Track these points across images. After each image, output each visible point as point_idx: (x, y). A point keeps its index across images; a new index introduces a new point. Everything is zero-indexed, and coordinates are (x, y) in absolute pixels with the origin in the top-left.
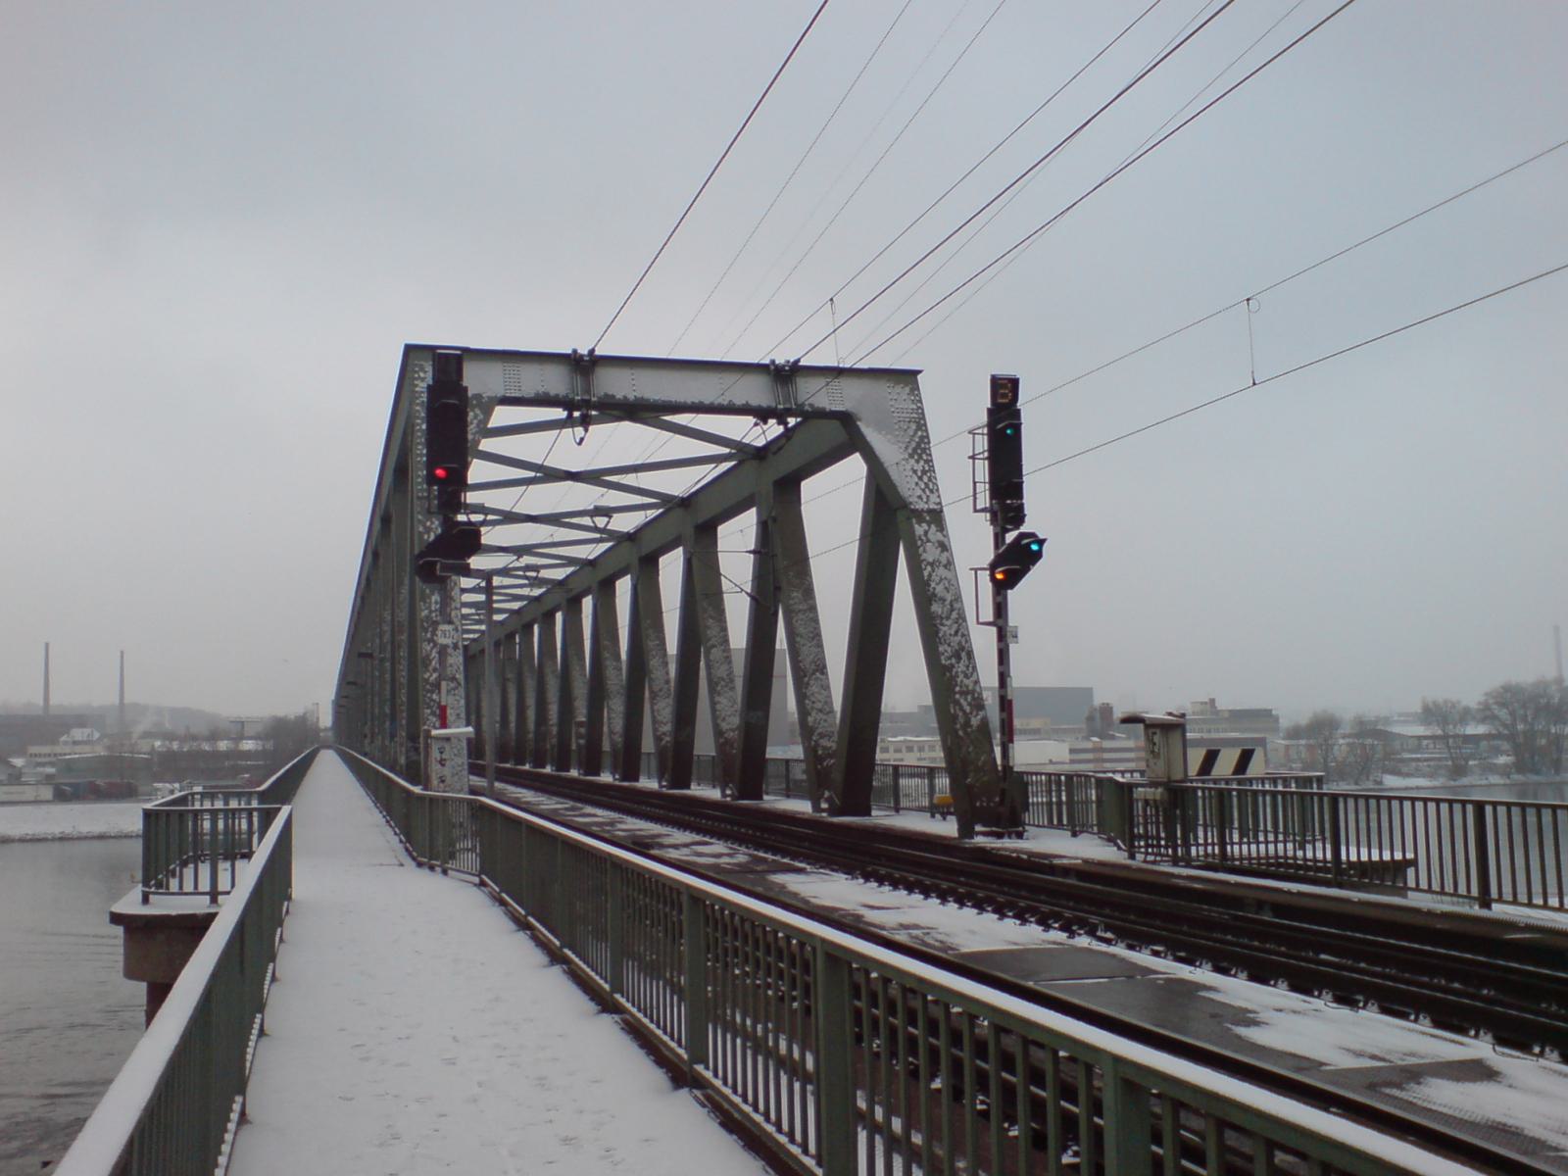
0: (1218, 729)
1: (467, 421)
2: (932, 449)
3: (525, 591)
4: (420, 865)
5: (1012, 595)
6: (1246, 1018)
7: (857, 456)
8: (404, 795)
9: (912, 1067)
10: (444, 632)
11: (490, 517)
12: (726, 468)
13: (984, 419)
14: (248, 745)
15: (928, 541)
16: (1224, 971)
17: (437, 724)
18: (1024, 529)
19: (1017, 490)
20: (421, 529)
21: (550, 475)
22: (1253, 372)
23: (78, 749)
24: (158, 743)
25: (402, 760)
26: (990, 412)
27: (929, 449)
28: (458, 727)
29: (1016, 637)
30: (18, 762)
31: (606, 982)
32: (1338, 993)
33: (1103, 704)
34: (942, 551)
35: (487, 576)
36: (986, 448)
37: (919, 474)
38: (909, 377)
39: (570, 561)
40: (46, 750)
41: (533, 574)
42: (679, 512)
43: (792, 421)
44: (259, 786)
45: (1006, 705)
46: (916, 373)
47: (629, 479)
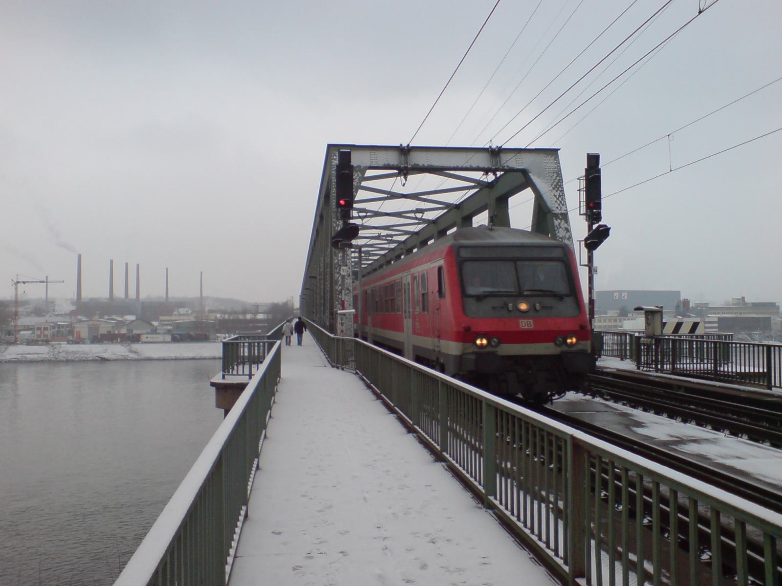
0: (737, 313)
1: (352, 185)
2: (564, 185)
3: (386, 246)
4: (333, 366)
5: (595, 253)
6: (639, 424)
7: (529, 190)
8: (327, 338)
9: (542, 460)
10: (343, 270)
11: (368, 214)
12: (473, 193)
13: (584, 173)
14: (260, 316)
15: (560, 227)
16: (634, 407)
17: (341, 308)
18: (600, 223)
19: (598, 206)
20: (334, 225)
21: (393, 196)
22: (671, 166)
23: (182, 317)
24: (218, 316)
25: (328, 324)
26: (586, 170)
27: (562, 185)
28: (350, 310)
29: (596, 271)
30: (155, 323)
31: (438, 445)
32: (684, 418)
33: (685, 299)
34: (567, 232)
35: (359, 247)
36: (584, 186)
37: (557, 197)
38: (554, 152)
39: (406, 233)
40: (167, 318)
41: (390, 238)
42: (454, 211)
43: (499, 174)
44: (268, 333)
45: (591, 301)
46: (557, 150)
47: (431, 197)
